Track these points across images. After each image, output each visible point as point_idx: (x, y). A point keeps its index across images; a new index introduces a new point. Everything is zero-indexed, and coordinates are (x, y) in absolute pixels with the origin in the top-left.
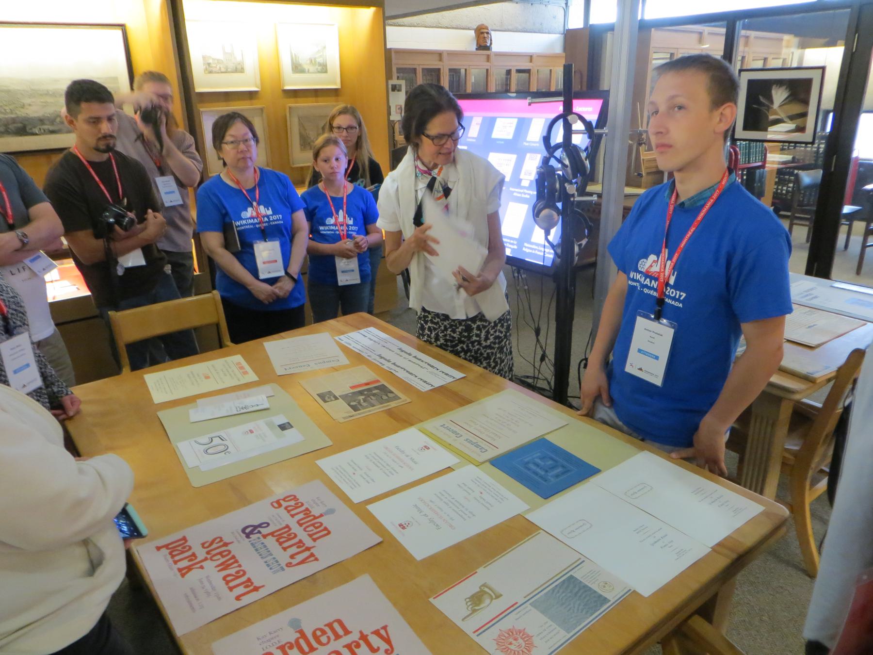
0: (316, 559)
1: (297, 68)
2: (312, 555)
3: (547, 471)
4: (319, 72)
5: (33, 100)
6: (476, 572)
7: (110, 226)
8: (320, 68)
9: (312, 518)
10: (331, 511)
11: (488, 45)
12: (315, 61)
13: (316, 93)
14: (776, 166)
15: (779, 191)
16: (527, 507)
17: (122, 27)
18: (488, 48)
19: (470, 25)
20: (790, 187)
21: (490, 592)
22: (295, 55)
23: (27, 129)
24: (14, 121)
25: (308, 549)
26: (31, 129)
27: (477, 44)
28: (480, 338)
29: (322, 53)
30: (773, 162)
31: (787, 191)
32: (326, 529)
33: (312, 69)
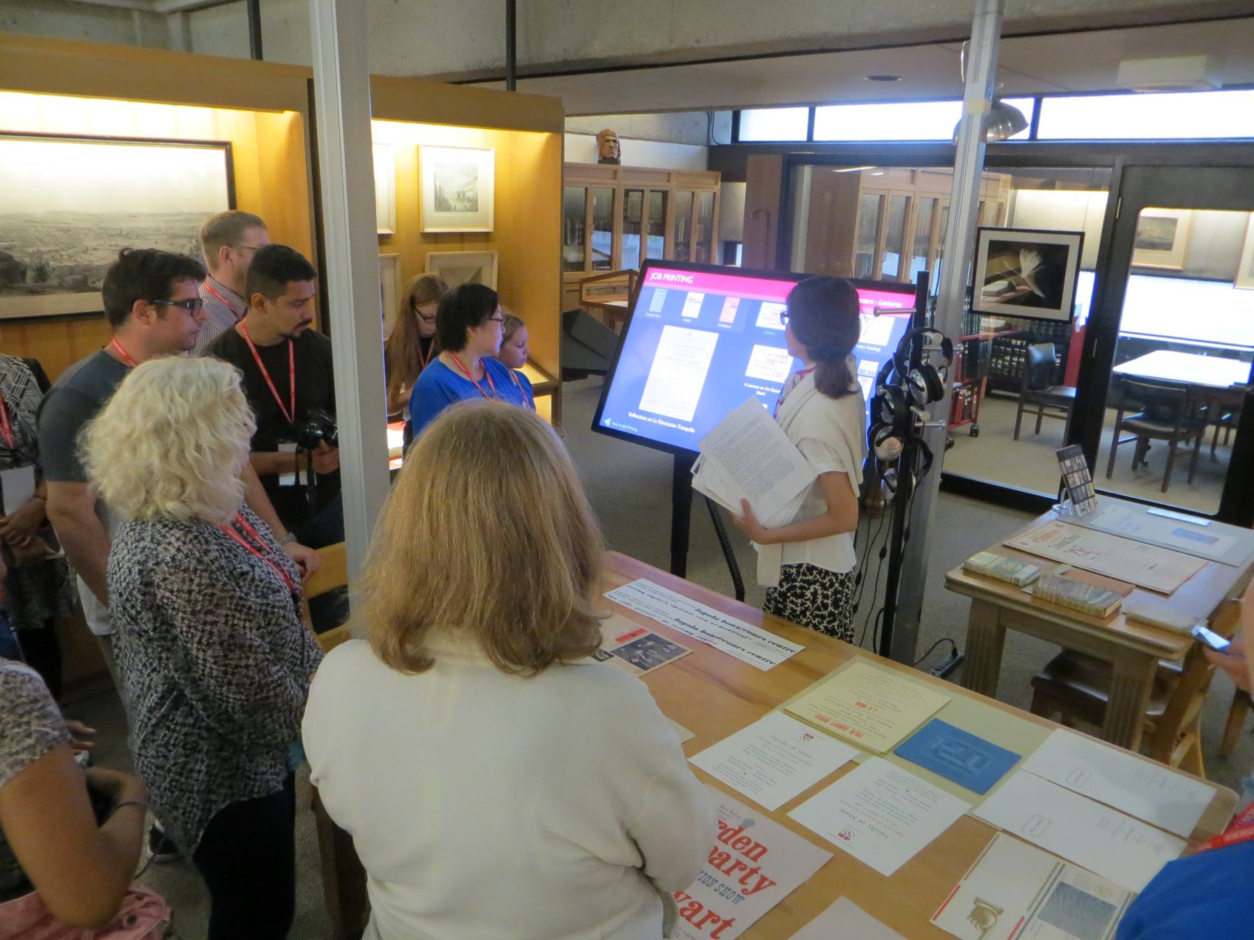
0: (772, 883)
1: (441, 204)
2: (763, 879)
3: (963, 761)
4: (468, 210)
5: (101, 242)
6: (959, 886)
7: (317, 438)
8: (469, 205)
9: (732, 832)
10: (750, 823)
11: (616, 157)
12: (464, 195)
13: (462, 237)
14: (992, 334)
15: (993, 365)
16: (970, 806)
17: (226, 146)
18: (616, 161)
19: (590, 129)
20: (1006, 361)
21: (989, 908)
22: (440, 188)
23: (89, 283)
24: (71, 271)
25: (754, 871)
26: (94, 283)
27: (600, 155)
28: (823, 594)
29: (472, 186)
30: (988, 329)
31: (1003, 365)
32: (757, 845)
33: (459, 206)
